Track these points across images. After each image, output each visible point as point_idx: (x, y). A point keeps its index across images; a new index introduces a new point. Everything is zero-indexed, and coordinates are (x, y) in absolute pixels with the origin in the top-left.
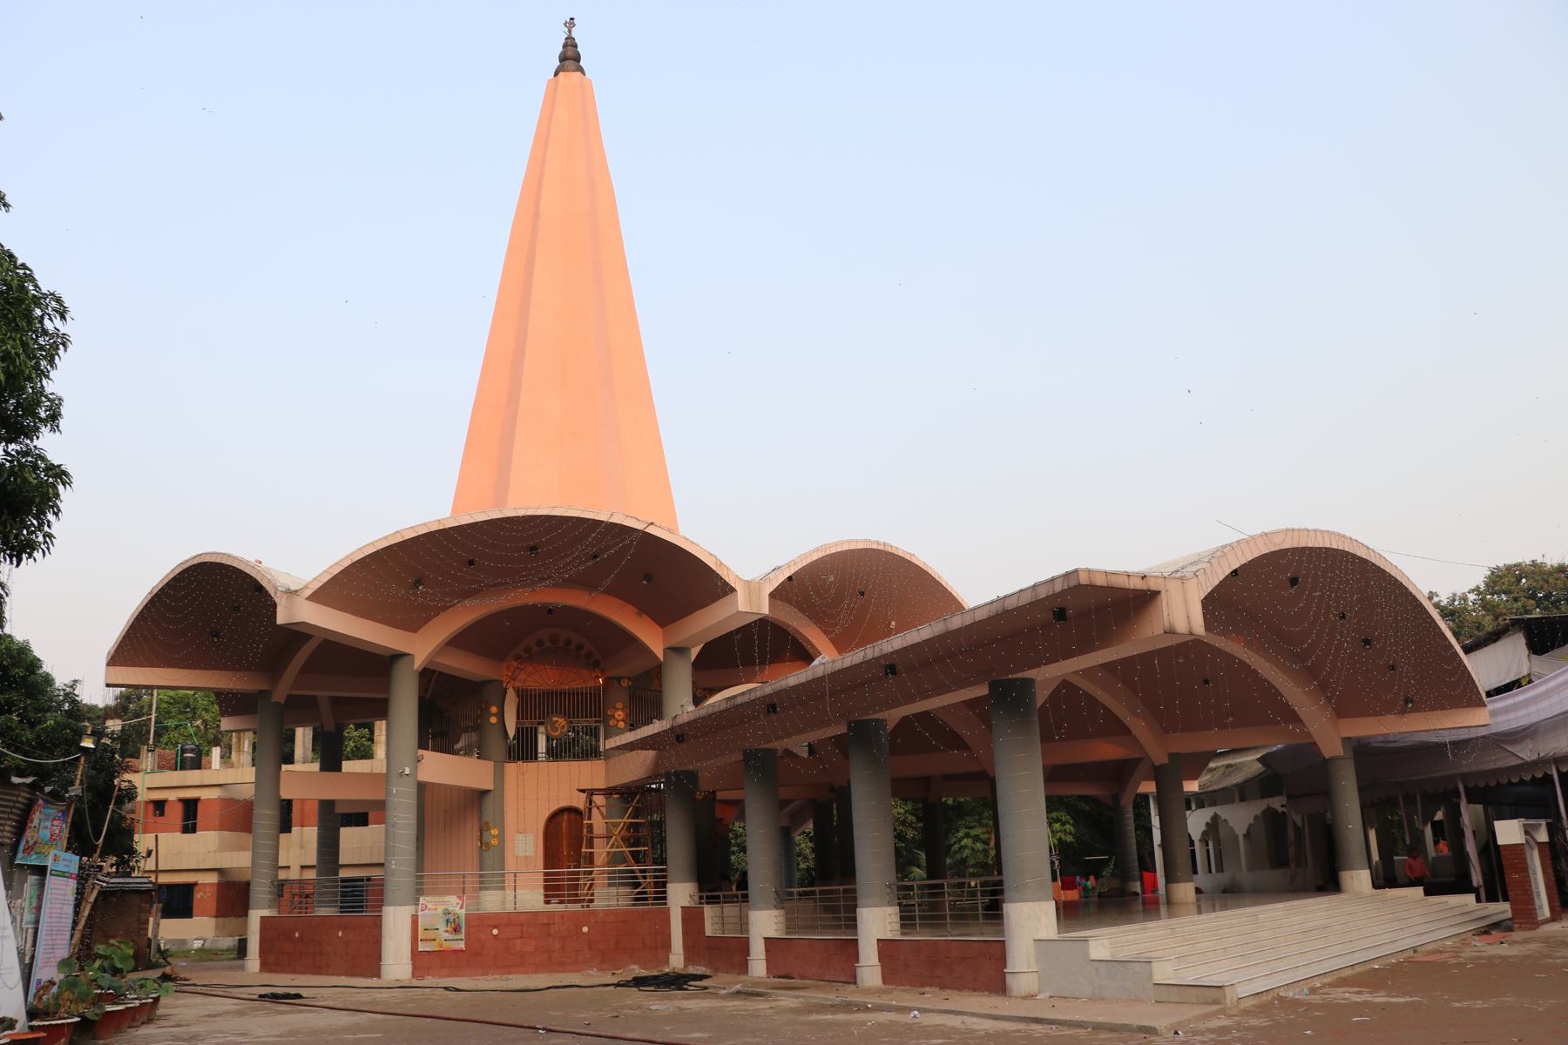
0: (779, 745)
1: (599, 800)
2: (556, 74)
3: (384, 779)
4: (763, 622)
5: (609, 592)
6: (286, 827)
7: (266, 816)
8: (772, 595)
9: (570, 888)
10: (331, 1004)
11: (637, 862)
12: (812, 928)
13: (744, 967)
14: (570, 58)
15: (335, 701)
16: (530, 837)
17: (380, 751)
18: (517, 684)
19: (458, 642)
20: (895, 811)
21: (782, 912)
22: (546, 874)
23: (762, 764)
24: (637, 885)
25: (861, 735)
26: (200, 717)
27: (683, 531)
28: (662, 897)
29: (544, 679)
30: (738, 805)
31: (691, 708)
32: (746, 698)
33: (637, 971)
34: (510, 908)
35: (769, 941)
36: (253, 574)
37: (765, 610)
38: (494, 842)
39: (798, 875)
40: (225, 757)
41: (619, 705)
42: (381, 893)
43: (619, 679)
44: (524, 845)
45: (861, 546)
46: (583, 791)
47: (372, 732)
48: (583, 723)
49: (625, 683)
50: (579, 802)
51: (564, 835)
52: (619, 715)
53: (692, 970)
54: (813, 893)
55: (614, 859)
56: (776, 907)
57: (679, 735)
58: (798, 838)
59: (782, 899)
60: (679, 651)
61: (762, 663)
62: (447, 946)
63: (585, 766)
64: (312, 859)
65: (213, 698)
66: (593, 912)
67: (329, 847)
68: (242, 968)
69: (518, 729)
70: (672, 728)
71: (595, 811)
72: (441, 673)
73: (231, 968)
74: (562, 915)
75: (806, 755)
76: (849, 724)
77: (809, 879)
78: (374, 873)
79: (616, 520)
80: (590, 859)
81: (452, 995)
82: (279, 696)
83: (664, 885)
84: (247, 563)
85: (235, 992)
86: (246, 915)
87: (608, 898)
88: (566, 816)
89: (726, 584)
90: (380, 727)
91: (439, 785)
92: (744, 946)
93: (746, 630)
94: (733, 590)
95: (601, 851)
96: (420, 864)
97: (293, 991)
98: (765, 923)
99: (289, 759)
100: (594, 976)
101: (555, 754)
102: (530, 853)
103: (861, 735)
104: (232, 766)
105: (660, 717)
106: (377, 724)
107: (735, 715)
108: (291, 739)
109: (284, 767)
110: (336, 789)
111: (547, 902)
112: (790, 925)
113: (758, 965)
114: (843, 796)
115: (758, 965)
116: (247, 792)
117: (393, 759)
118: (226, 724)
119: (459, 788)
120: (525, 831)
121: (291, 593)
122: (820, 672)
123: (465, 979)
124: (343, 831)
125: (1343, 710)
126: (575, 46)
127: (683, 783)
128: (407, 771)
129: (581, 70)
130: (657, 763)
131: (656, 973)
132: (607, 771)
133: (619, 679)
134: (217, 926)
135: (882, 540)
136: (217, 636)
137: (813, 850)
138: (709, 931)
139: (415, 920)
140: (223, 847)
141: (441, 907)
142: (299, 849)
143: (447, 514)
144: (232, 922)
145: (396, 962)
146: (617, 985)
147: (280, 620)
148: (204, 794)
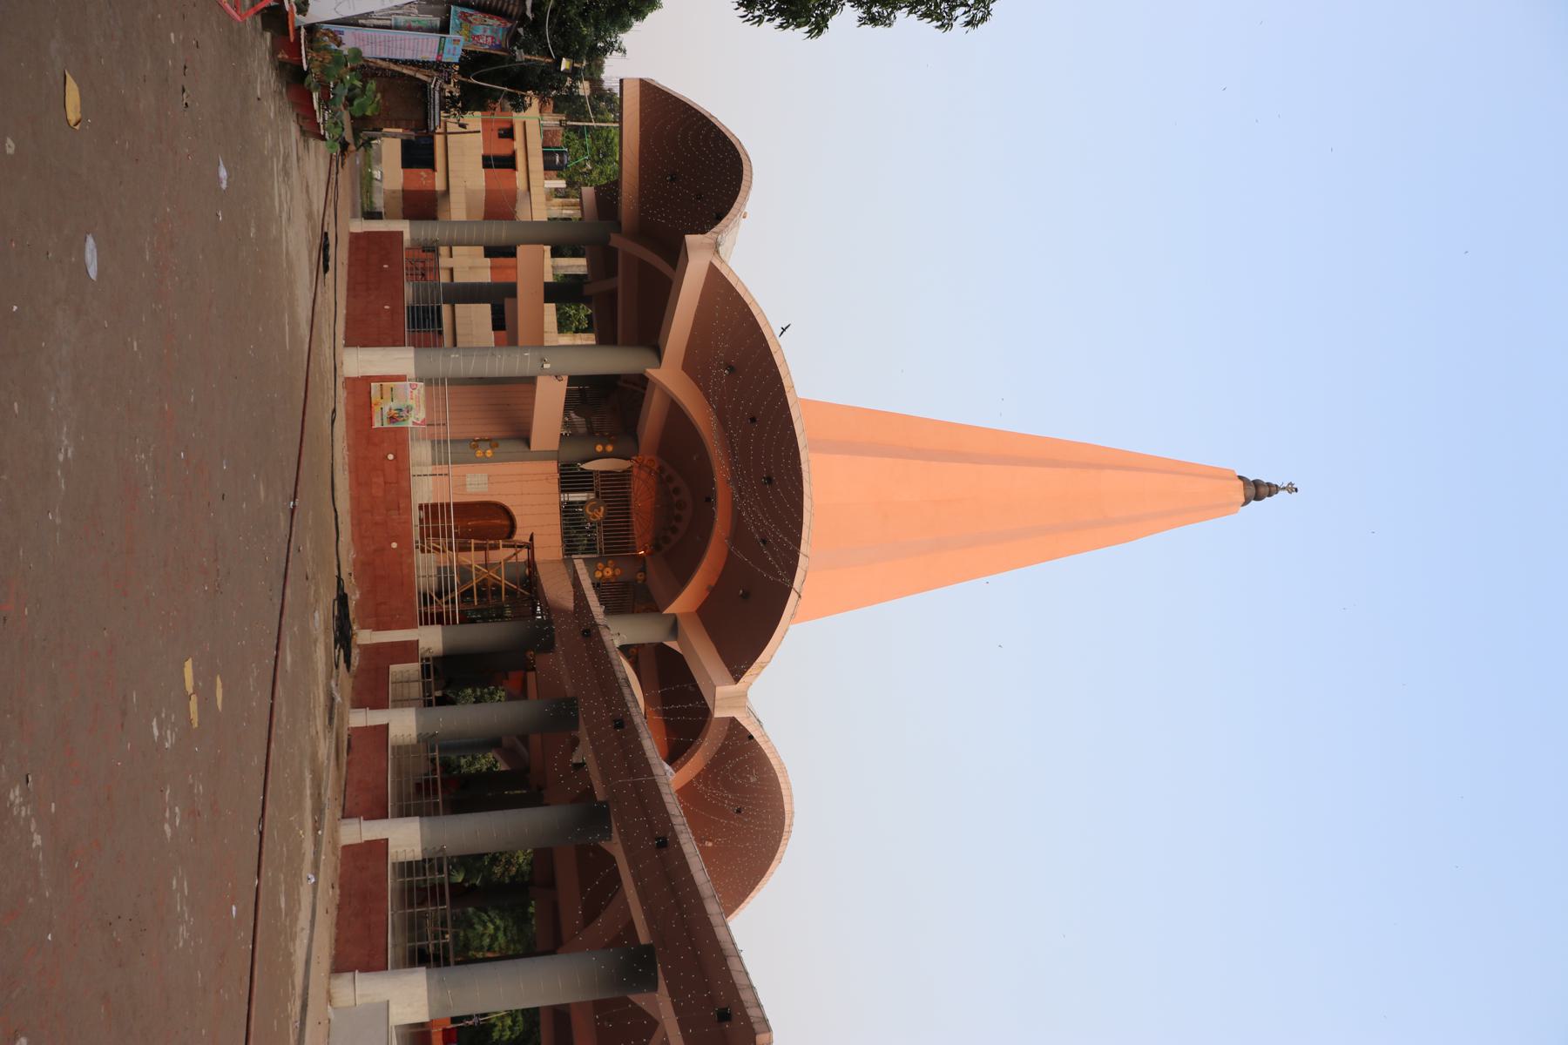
0: (582, 732)
1: (523, 555)
2: (1241, 478)
3: (538, 344)
4: (706, 712)
6: (490, 252)
7: (500, 232)
8: (733, 720)
9: (435, 529)
10: (319, 300)
11: (462, 595)
12: (399, 772)
13: (359, 703)
14: (1258, 490)
16: (484, 488)
17: (566, 339)
18: (635, 470)
19: (675, 411)
20: (520, 853)
22: (448, 505)
23: (563, 716)
24: (439, 595)
25: (595, 816)
26: (594, 167)
28: (427, 620)
29: (642, 496)
30: (523, 694)
31: (617, 643)
32: (628, 697)
33: (354, 598)
38: (479, 453)
39: (453, 757)
40: (557, 193)
41: (618, 572)
42: (427, 345)
43: (643, 570)
44: (478, 482)
45: (787, 807)
47: (584, 331)
48: (599, 537)
49: (640, 576)
50: (521, 536)
51: (487, 522)
52: (608, 572)
53: (355, 652)
55: (465, 572)
56: (419, 735)
57: (590, 632)
58: (490, 755)
60: (674, 629)
61: (665, 713)
62: (376, 410)
64: (458, 279)
67: (472, 294)
68: (354, 216)
70: (596, 625)
71: (512, 551)
73: (354, 205)
74: (409, 522)
75: (574, 760)
77: (447, 766)
80: (463, 548)
81: (328, 416)
82: (616, 240)
83: (440, 622)
84: (743, 204)
85: (331, 210)
87: (426, 567)
88: (507, 523)
89: (743, 673)
90: (589, 339)
91: (533, 398)
92: (380, 704)
94: (737, 680)
95: (473, 558)
96: (456, 382)
97: (331, 264)
98: (403, 724)
100: (348, 554)
101: (568, 510)
102: (470, 489)
103: (595, 816)
105: (607, 612)
106: (592, 336)
107: (611, 686)
108: (575, 254)
109: (548, 248)
112: (401, 750)
113: (361, 719)
114: (534, 799)
115: (361, 719)
116: (523, 214)
117: (559, 354)
118: (588, 192)
121: (716, 247)
122: (657, 771)
123: (344, 429)
126: (1270, 495)
127: (543, 639)
128: (547, 366)
129: (1246, 503)
130: (562, 611)
131: (352, 616)
133: (643, 570)
136: (672, 180)
137: (479, 772)
139: (401, 378)
141: (410, 403)
142: (470, 266)
144: (398, 205)
145: (360, 362)
146: (339, 578)
147: (689, 238)
148: (520, 175)
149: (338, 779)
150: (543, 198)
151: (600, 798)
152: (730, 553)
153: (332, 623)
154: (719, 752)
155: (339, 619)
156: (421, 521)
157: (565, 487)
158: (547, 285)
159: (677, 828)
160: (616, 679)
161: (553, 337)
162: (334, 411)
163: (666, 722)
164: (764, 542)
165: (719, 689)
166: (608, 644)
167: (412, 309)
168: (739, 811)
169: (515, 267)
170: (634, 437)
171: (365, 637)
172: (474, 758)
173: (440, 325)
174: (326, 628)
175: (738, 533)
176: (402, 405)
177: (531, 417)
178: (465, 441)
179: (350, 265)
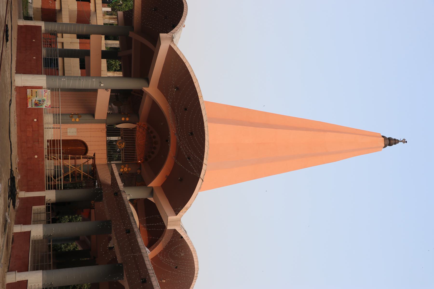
0: (113, 235)
1: (91, 162)
2: (383, 137)
3: (99, 76)
4: (164, 227)
5: (175, 164)
6: (79, 37)
7: (83, 29)
8: (175, 230)
9: (54, 150)
10: (4, 54)
11: (65, 178)
12: (34, 251)
13: (18, 222)
14: (390, 142)
15: (130, 56)
16: (75, 134)
17: (110, 74)
18: (138, 128)
19: (154, 104)
20: (86, 285)
21: (42, 238)
22: (60, 140)
23: (105, 228)
24: (55, 177)
25: (117, 269)
26: (123, 3)
27: (200, 193)
28: (50, 188)
29: (140, 139)
30: (89, 218)
31: (128, 198)
32: (132, 221)
33: (18, 178)
34: (45, 126)
35: (29, 232)
36: (179, 24)
37: (169, 228)
38: (73, 120)
39: (59, 244)
40: (107, 13)
41: (130, 169)
42: (52, 74)
43: (140, 169)
44: (72, 132)
45: (196, 266)
46: (94, 155)
47: (118, 71)
48: (123, 155)
49: (138, 171)
50: (90, 154)
51: (76, 148)
52: (126, 169)
53: (17, 201)
54: (50, 251)
55: (66, 168)
56: (44, 236)
57: (118, 194)
58: (75, 243)
59: (47, 238)
60: (152, 193)
61: (147, 227)
62: (29, 101)
63: (105, 156)
64: (66, 47)
65: (131, 8)
66: (43, 160)
67: (71, 54)
68: (20, 18)
69: (119, 129)
70: (120, 191)
71: (86, 160)
72: (142, 98)
73: (19, 14)
74: (43, 147)
75: (109, 246)
76: (121, 264)
77: (56, 249)
78: (60, 72)
79: (204, 167)
80: (66, 158)
81: (8, 103)
82: (131, 34)
83: (55, 188)
84: (183, 22)
85: (9, 15)
86: (42, 20)
87: (49, 166)
88: (84, 148)
89: (179, 211)
90: (120, 74)
91: (96, 97)
92: (27, 222)
93: (161, 220)
94: (177, 214)
95: (69, 163)
96: (63, 90)
97: (9, 38)
98: (37, 231)
99: (107, 38)
100: (15, 160)
101: (110, 144)
102: (69, 134)
103: (117, 269)
104: (104, 16)
105: (125, 186)
106: (121, 73)
107: (125, 216)
108: (115, 39)
109: (103, 37)
110: (94, 55)
111: (48, 141)
112: (36, 242)
113: (18, 229)
114: (92, 262)
115: (18, 229)
116: (93, 22)
117: (107, 80)
118: (120, 13)
119: (95, 105)
120: (77, 132)
121: (172, 39)
122: (143, 251)
123: (15, 108)
124: (78, 59)
126: (395, 144)
127: (98, 196)
128: (102, 85)
129: (385, 146)
130: (106, 185)
131: (16, 186)
132: (103, 165)
133: (140, 169)
134: (37, 8)
135: (198, 275)
136: (155, 10)
137: (69, 250)
138: (34, 208)
139: (40, 88)
140: (70, 12)
141: (46, 99)
142: (70, 42)
143: (204, 100)
144: (40, 15)
145: (22, 80)
146: (11, 170)
147: (161, 35)
148: (92, 4)
149: (7, 255)
150: (102, 15)
151: (119, 262)
152: (175, 162)
153: (7, 189)
154: (169, 243)
155: (11, 187)
156: (48, 147)
157: (108, 135)
158: (103, 52)
159: (151, 275)
160: (127, 213)
161: (105, 73)
162: (11, 100)
163: (148, 231)
164: (189, 159)
165: (170, 218)
166: (124, 199)
167: (45, 59)
168: (176, 268)
169: (90, 43)
170: (138, 116)
171: (22, 194)
172: (68, 245)
173: (57, 66)
174: (5, 191)
175: (179, 155)
176: (40, 99)
177: (95, 105)
178: (65, 113)
179: (18, 39)
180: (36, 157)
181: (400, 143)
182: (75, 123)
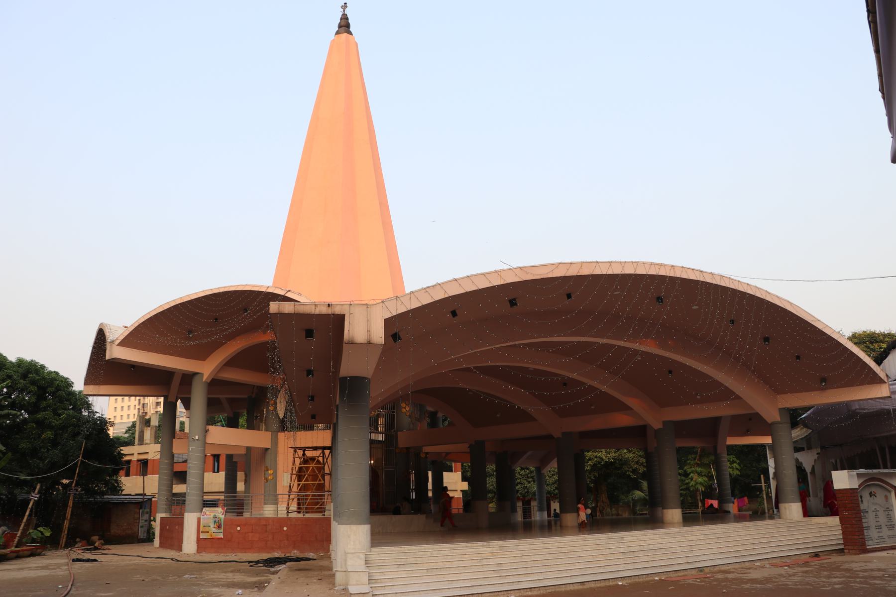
14: (344, 26)
33: (265, 556)
62: (215, 535)
125: (778, 389)
126: (347, 19)
129: (350, 33)
145: (189, 545)
176: (212, 521)
180: (285, 529)
181: (347, 12)
182: (275, 474)
